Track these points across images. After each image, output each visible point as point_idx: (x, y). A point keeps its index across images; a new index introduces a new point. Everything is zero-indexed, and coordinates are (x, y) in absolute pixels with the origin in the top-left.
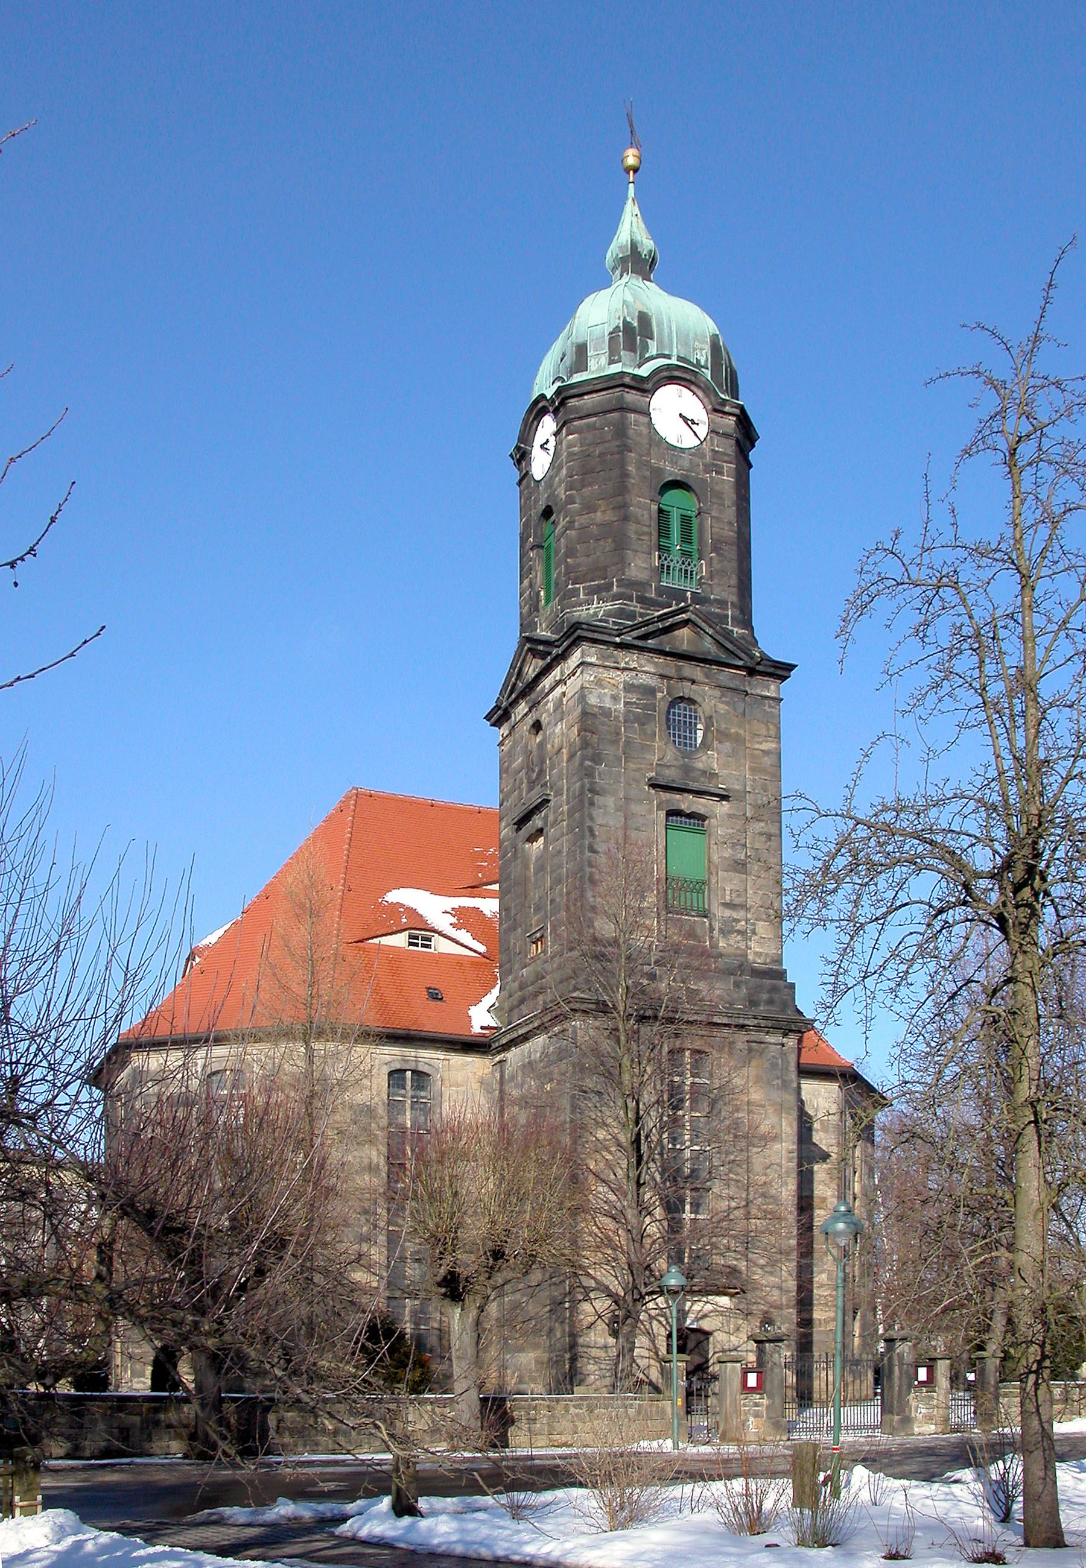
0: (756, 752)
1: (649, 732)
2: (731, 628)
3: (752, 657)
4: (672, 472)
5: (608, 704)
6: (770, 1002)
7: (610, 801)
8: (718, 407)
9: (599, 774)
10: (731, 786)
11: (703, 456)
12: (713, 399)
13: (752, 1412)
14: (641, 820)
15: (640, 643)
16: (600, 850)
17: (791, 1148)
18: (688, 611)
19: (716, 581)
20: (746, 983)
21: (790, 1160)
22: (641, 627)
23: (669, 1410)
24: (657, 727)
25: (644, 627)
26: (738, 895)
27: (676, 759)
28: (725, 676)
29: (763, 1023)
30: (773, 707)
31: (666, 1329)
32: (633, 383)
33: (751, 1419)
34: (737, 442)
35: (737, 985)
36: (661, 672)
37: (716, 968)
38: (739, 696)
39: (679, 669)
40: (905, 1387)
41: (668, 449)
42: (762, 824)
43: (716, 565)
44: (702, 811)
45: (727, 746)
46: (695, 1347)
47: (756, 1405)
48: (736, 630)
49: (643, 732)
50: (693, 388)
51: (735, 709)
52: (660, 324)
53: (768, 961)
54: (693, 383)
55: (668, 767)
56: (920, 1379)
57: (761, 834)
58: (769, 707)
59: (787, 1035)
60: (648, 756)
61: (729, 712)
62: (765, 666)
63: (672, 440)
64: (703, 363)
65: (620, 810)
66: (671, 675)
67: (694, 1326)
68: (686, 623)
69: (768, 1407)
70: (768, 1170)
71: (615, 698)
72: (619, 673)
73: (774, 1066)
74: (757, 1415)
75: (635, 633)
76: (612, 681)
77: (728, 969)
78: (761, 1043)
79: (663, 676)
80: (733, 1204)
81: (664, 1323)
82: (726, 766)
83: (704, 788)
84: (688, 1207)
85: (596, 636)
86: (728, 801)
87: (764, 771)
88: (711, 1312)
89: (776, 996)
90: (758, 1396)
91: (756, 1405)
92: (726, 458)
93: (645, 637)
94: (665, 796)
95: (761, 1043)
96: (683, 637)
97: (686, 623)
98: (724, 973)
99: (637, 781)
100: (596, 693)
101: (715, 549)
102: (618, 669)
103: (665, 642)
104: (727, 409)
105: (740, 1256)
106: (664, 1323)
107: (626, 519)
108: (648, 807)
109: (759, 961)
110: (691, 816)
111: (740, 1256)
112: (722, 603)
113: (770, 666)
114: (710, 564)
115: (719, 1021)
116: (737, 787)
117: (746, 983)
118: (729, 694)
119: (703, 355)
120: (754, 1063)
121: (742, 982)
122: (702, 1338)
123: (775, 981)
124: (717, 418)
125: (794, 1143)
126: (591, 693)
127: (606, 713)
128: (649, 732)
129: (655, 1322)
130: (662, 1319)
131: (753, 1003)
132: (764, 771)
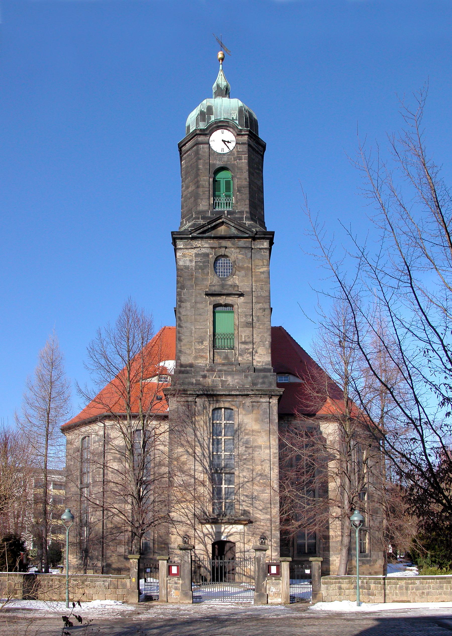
0: (257, 273)
1: (206, 272)
2: (244, 222)
3: (252, 232)
4: (219, 164)
5: (188, 263)
6: (263, 383)
7: (188, 305)
8: (239, 133)
9: (184, 294)
10: (245, 290)
11: (234, 154)
12: (236, 130)
13: (173, 587)
14: (202, 311)
15: (200, 235)
16: (184, 326)
17: (275, 451)
18: (222, 218)
19: (239, 204)
20: (251, 375)
21: (275, 457)
22: (200, 229)
23: (128, 584)
24: (210, 270)
25: (202, 228)
26: (249, 338)
27: (218, 282)
28: (242, 243)
29: (257, 393)
30: (265, 252)
31: (212, 541)
32: (200, 133)
33: (173, 591)
34: (249, 145)
35: (246, 377)
36: (211, 246)
37: (236, 370)
38: (249, 250)
39: (220, 243)
40: (261, 577)
41: (217, 155)
42: (261, 305)
43: (239, 197)
44: (230, 302)
45: (243, 273)
46: (229, 550)
47: (176, 583)
48: (247, 222)
49: (203, 273)
50: (228, 128)
51: (246, 256)
52: (216, 109)
53: (264, 364)
54: (227, 126)
55: (214, 286)
56: (272, 572)
57: (260, 309)
58: (263, 253)
59: (271, 397)
60: (205, 283)
61: (243, 258)
62: (260, 235)
63: (219, 151)
64: (235, 118)
65: (193, 308)
66: (215, 246)
67: (225, 540)
68: (223, 223)
69: (182, 585)
70: (263, 463)
71: (191, 261)
72: (193, 250)
73: (265, 413)
74: (176, 589)
75: (198, 232)
76: (189, 254)
77: (242, 370)
78: (258, 402)
79: (212, 248)
80: (246, 480)
81: (211, 538)
82: (242, 281)
83: (229, 292)
84: (223, 482)
85: (181, 236)
86: (243, 296)
87: (262, 281)
88: (235, 532)
89: (266, 380)
90: (176, 579)
91: (176, 583)
92: (244, 153)
93: (204, 232)
94: (213, 299)
95: (258, 402)
96: (222, 230)
97: (223, 223)
98: (240, 372)
99: (200, 294)
100: (182, 260)
101: (239, 191)
102: (192, 248)
103: (213, 233)
104: (243, 133)
105: (249, 505)
106: (211, 538)
107: (198, 187)
108: (205, 305)
109: (259, 365)
110: (226, 305)
111: (249, 505)
112: (241, 212)
113: (262, 234)
114: (236, 198)
115: (235, 393)
116: (248, 290)
117: (251, 375)
118: (244, 250)
119: (235, 115)
120: (254, 412)
121: (248, 375)
122: (232, 545)
123: (265, 373)
124: (240, 138)
125: (277, 449)
126: (180, 260)
127: (187, 268)
128: (206, 272)
129: (206, 538)
130: (210, 536)
131: (254, 384)
132: (262, 281)
